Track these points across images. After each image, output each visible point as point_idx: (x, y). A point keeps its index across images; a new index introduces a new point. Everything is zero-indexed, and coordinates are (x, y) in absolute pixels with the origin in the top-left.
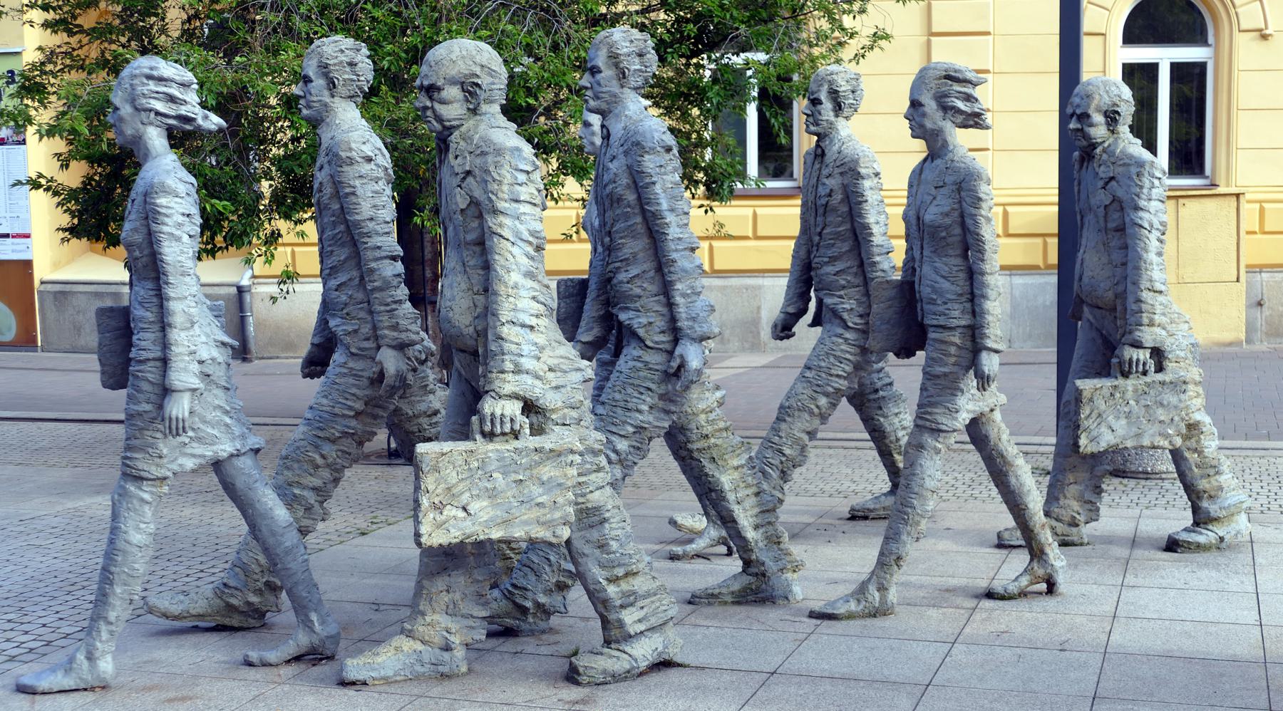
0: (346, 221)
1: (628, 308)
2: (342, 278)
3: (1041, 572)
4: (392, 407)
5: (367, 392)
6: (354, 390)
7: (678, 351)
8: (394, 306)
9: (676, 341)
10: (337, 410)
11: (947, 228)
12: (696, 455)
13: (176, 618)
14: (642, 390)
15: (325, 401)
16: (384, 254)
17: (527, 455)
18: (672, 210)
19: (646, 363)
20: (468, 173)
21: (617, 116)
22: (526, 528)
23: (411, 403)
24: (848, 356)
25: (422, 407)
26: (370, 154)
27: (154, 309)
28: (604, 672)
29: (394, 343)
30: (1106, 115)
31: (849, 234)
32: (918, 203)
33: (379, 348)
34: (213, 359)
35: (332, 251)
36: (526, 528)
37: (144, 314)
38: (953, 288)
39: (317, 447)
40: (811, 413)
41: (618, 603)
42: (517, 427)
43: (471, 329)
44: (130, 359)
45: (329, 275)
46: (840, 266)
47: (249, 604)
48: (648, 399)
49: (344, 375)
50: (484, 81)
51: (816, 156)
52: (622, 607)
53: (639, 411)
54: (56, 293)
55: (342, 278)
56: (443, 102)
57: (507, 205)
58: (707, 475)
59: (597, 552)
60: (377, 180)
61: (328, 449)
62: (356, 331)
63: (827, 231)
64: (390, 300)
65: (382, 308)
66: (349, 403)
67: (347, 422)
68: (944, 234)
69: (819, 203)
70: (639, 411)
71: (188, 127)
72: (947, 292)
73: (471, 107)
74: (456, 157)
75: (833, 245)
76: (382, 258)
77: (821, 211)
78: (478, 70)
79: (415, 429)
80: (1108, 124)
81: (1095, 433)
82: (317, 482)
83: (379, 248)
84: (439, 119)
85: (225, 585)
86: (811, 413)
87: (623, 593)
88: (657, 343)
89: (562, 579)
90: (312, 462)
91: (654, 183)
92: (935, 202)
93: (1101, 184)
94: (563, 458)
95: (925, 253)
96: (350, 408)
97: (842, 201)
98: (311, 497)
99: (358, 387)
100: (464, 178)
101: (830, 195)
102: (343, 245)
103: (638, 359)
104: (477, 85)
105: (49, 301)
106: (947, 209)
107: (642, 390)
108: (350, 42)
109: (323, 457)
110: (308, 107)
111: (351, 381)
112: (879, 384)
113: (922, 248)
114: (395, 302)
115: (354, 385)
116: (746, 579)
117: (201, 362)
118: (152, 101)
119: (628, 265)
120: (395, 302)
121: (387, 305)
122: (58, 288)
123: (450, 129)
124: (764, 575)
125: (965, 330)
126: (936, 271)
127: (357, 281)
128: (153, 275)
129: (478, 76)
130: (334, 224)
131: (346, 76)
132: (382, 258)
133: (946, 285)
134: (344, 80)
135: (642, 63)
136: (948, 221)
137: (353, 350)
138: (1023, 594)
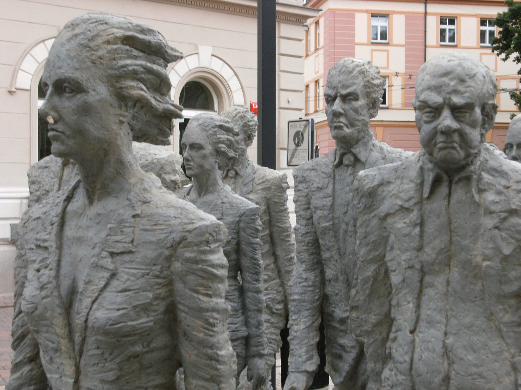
68: (138, 348)
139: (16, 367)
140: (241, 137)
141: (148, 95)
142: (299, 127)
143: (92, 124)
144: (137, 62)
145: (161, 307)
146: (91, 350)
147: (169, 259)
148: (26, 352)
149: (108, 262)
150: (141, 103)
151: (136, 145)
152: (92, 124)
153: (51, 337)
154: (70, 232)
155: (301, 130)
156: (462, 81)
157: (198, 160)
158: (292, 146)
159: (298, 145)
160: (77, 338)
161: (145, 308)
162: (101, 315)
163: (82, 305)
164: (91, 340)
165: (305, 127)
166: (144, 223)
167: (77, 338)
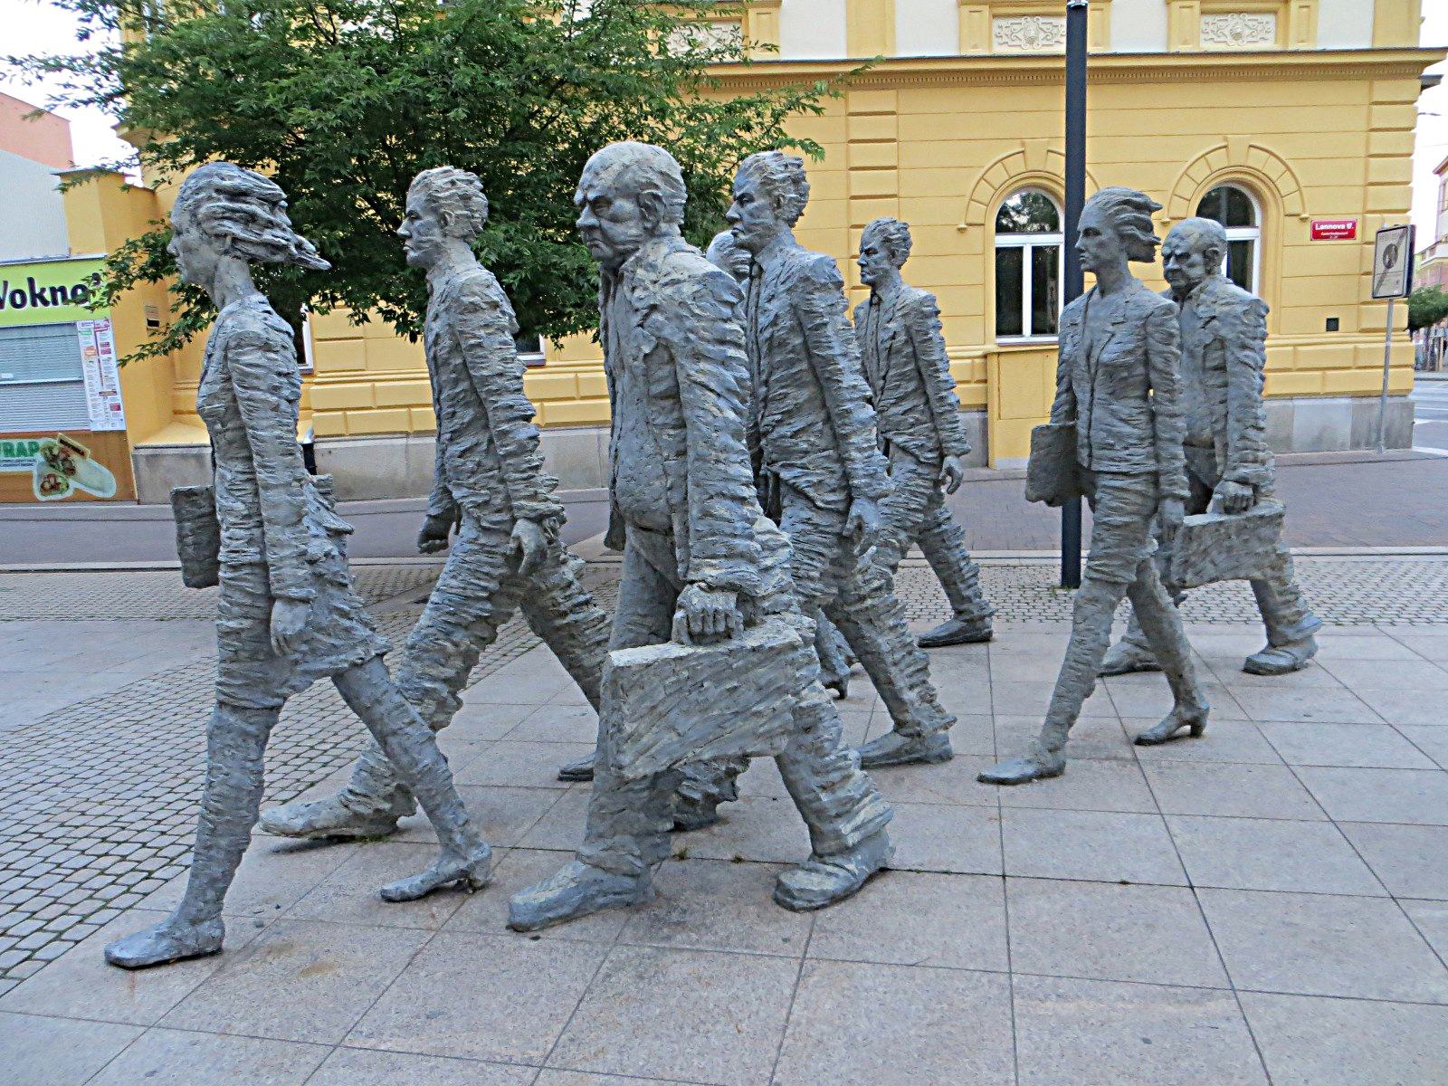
0: (470, 377)
1: (792, 466)
2: (466, 442)
3: (1188, 715)
4: (529, 585)
5: (503, 571)
6: (486, 569)
7: (854, 511)
8: (530, 473)
9: (850, 500)
10: (469, 593)
11: (1128, 367)
12: (853, 617)
13: (298, 835)
14: (813, 556)
15: (454, 583)
16: (517, 414)
17: (743, 657)
18: (845, 355)
19: (816, 525)
20: (654, 308)
21: (771, 250)
22: (741, 743)
23: (544, 577)
24: (922, 490)
25: (554, 579)
26: (496, 299)
27: (249, 499)
28: (823, 893)
29: (533, 515)
30: (1204, 254)
31: (915, 374)
32: (1087, 342)
33: (514, 520)
34: (327, 555)
35: (454, 413)
36: (741, 743)
37: (231, 506)
38: (1136, 431)
39: (448, 634)
40: (894, 548)
41: (833, 813)
42: (732, 625)
43: (662, 502)
44: (219, 563)
45: (451, 440)
46: (906, 405)
47: (377, 811)
48: (819, 565)
49: (475, 552)
50: (664, 190)
51: (871, 304)
52: (838, 816)
53: (811, 579)
54: (147, 457)
55: (466, 442)
56: (615, 219)
57: (710, 347)
58: (863, 637)
59: (810, 757)
60: (502, 330)
61: (458, 636)
62: (486, 503)
63: (891, 373)
64: (525, 466)
65: (518, 475)
66: (482, 583)
67: (479, 605)
68: (1125, 374)
69: (881, 347)
70: (811, 579)
71: (278, 258)
72: (1129, 436)
73: (649, 225)
74: (633, 289)
75: (898, 387)
76: (516, 419)
77: (884, 354)
78: (657, 180)
79: (549, 603)
80: (1206, 264)
81: (1199, 568)
82: (449, 672)
83: (511, 407)
84: (609, 241)
85: (351, 792)
86: (894, 548)
87: (839, 800)
88: (828, 503)
89: (732, 765)
90: (443, 649)
91: (825, 324)
92: (1115, 340)
93: (1201, 323)
94: (782, 657)
95: (1096, 395)
96: (484, 589)
97: (906, 342)
98: (444, 691)
99: (492, 565)
100: (647, 316)
101: (893, 338)
102: (467, 405)
103: (807, 521)
104: (656, 197)
105: (142, 464)
106: (1131, 346)
107: (813, 556)
108: (459, 174)
109: (456, 645)
110: (417, 248)
111: (483, 558)
112: (942, 518)
113: (1093, 390)
114: (531, 468)
115: (486, 563)
116: (899, 740)
117: (312, 562)
118: (226, 222)
119: (791, 417)
120: (531, 468)
121: (524, 471)
122: (149, 452)
123: (624, 255)
124: (919, 735)
125: (1149, 477)
126: (1113, 413)
127: (484, 446)
128: (244, 453)
129: (657, 187)
130: (456, 382)
131: (459, 212)
132: (516, 419)
133: (1127, 429)
134: (457, 216)
135: (796, 191)
136: (1129, 359)
137: (484, 524)
138: (1170, 738)
139: (1058, 395)
140: (882, 253)
141: (1138, 233)
142: (1392, 239)
143: (1212, 414)
144: (1129, 214)
145: (1140, 352)
146: (1100, 377)
147: (1144, 325)
148: (1064, 386)
149: (1111, 328)
150: (1133, 238)
151: (1131, 264)
152: (1212, 414)
153: (1080, 371)
154: (1090, 312)
155: (1394, 242)
156: (1182, 239)
157: (1093, 250)
158: (1381, 268)
159: (1389, 266)
160: (1093, 371)
161: (1130, 352)
162: (1105, 357)
163: (1095, 353)
164: (1100, 372)
165: (1401, 237)
166: (1131, 305)
167: (1093, 371)
